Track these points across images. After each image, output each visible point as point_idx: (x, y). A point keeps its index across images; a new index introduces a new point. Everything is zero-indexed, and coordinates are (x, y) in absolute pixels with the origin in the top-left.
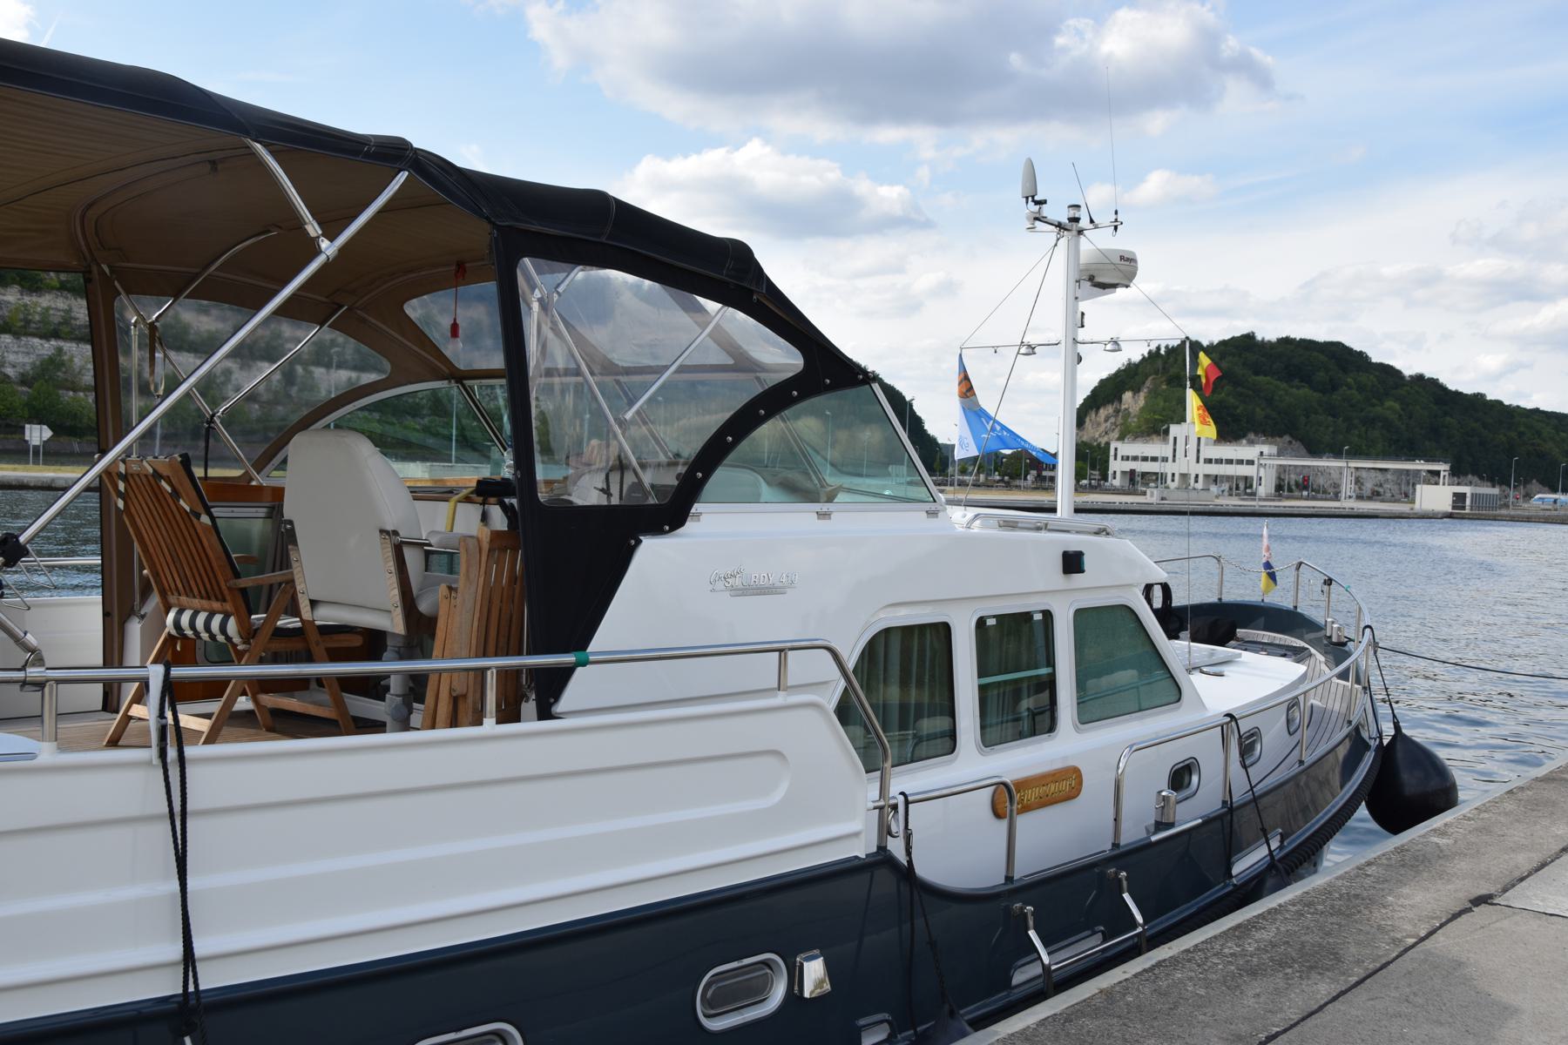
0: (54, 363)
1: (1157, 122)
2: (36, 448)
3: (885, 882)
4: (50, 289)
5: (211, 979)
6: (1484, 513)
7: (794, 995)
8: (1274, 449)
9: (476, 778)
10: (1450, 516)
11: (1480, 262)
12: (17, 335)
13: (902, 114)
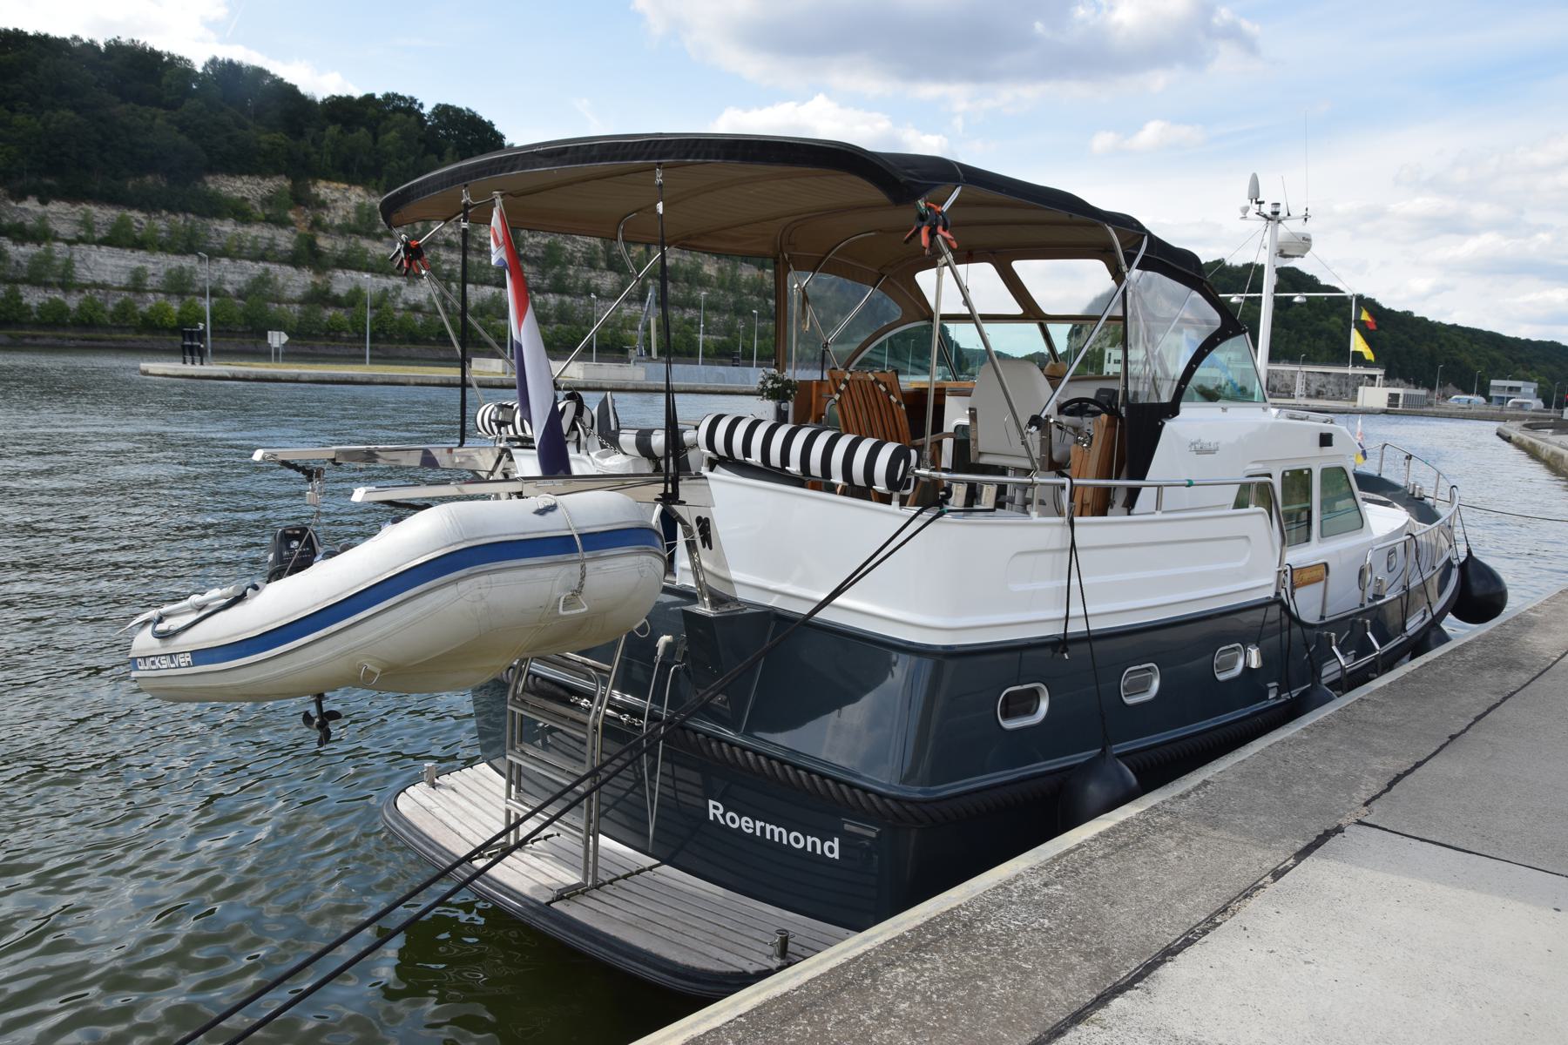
0: (263, 281)
1: (1158, 80)
2: (277, 350)
3: (1275, 612)
4: (258, 221)
5: (1095, 625)
6: (1414, 410)
7: (1247, 668)
8: (1239, 356)
9: (290, 656)
10: (1386, 412)
11: (1419, 200)
12: (233, 258)
13: (940, 73)
